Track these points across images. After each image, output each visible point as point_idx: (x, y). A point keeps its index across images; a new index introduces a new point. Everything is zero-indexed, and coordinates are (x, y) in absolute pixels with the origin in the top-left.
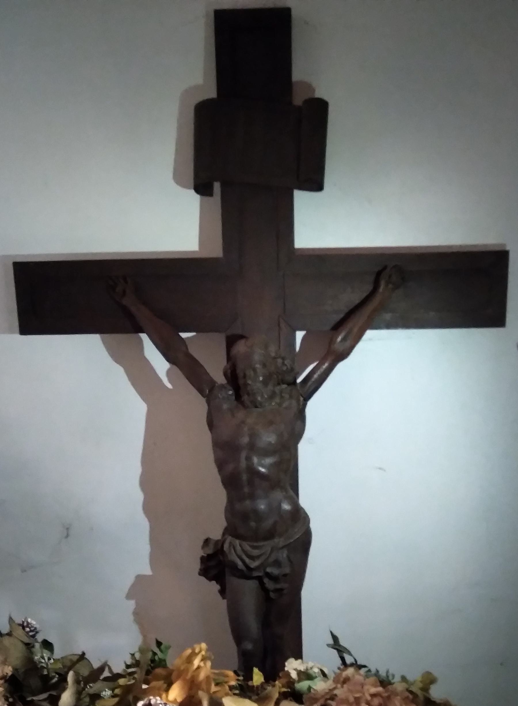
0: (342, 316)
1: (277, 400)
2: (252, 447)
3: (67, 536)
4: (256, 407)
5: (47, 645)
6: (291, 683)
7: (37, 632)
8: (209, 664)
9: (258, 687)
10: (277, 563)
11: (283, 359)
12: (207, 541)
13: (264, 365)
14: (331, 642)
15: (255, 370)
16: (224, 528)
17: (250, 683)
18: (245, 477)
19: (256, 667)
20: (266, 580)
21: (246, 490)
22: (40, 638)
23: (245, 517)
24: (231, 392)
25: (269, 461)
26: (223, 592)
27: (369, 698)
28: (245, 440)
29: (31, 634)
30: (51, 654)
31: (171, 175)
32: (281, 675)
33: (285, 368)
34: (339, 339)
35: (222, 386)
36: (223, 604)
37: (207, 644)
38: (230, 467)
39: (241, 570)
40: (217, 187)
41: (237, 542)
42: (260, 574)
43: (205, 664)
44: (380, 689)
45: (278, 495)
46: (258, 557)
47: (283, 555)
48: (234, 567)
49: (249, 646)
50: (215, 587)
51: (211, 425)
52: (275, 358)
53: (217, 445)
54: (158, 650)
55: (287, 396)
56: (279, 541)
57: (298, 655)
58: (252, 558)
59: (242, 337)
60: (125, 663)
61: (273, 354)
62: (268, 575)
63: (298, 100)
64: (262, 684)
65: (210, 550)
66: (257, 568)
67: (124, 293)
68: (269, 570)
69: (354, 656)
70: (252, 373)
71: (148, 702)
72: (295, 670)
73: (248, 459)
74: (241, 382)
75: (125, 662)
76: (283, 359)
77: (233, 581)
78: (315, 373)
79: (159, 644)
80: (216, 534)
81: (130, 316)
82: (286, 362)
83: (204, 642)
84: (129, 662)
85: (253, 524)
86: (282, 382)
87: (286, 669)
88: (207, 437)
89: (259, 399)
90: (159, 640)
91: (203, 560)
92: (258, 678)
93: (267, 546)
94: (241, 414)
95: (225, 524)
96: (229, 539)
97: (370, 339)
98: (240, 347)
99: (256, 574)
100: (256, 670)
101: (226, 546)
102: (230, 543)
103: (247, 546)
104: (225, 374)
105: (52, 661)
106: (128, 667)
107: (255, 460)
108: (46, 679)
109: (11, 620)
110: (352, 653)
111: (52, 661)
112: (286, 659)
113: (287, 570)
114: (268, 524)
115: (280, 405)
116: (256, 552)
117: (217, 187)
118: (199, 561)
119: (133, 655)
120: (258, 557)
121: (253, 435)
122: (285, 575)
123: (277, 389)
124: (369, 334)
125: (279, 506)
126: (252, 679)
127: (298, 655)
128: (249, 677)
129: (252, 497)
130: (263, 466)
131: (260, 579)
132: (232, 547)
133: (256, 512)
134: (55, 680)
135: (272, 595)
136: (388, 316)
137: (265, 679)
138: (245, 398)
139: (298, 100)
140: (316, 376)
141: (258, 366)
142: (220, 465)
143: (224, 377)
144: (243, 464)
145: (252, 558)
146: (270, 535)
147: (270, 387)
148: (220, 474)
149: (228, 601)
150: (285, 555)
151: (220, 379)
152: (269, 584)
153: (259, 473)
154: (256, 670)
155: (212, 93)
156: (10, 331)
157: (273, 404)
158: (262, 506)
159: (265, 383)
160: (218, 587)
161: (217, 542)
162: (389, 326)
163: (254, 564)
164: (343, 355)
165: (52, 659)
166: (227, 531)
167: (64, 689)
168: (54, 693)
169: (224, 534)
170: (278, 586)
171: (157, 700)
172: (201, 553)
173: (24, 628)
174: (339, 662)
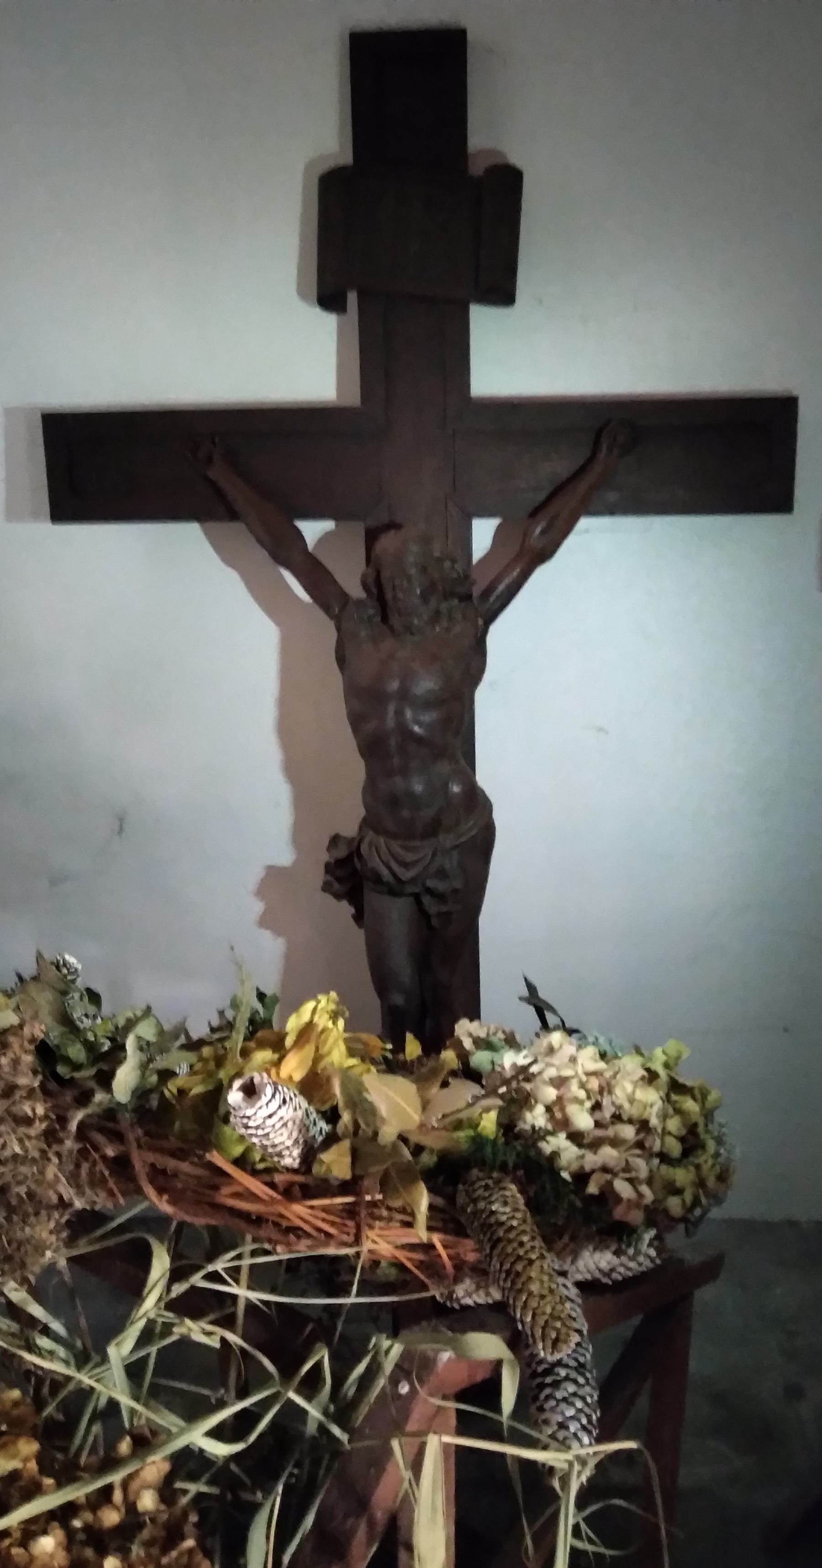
0: (542, 496)
1: (445, 623)
2: (404, 695)
3: (121, 830)
4: (412, 634)
5: (94, 997)
6: (463, 1056)
7: (78, 976)
8: (341, 1023)
9: (412, 1062)
10: (442, 874)
11: (454, 561)
12: (335, 840)
13: (423, 570)
14: (525, 992)
15: (409, 579)
16: (360, 819)
17: (401, 1057)
18: (393, 742)
19: (411, 1032)
20: (426, 900)
21: (396, 761)
22: (80, 983)
23: (394, 802)
24: (371, 612)
25: (427, 717)
26: (359, 918)
27: (584, 1078)
28: (394, 685)
29: (69, 978)
30: (97, 1010)
31: (293, 287)
32: (448, 1043)
33: (455, 576)
34: (538, 531)
35: (359, 603)
36: (358, 936)
37: (338, 995)
38: (370, 726)
39: (387, 884)
40: (352, 298)
41: (382, 840)
42: (417, 890)
43: (335, 1023)
44: (601, 1065)
45: (444, 768)
46: (414, 863)
47: (451, 863)
48: (378, 879)
49: (398, 999)
50: (346, 909)
51: (341, 660)
52: (440, 560)
53: (352, 691)
54: (261, 1005)
55: (459, 617)
56: (446, 840)
57: (474, 1014)
58: (406, 865)
59: (393, 526)
60: (209, 1023)
61: (437, 554)
62: (429, 891)
63: (477, 168)
64: (419, 1058)
65: (342, 852)
66: (413, 881)
67: (210, 460)
68: (430, 883)
69: (560, 1015)
70: (405, 584)
71: (248, 1082)
72: (470, 1035)
73: (399, 713)
74: (389, 595)
75: (258, 989)
76: (454, 561)
77: (373, 899)
78: (499, 583)
79: (261, 996)
80: (350, 829)
81: (219, 493)
82: (456, 566)
83: (333, 990)
84: (216, 1022)
85: (406, 813)
86: (447, 595)
87: (456, 1034)
88: (336, 680)
89: (416, 621)
90: (262, 989)
91: (329, 868)
92: (413, 1048)
93: (425, 850)
94: (388, 644)
95: (362, 812)
96: (370, 835)
97: (587, 531)
98: (387, 543)
99: (410, 889)
100: (409, 1037)
101: (364, 848)
102: (370, 844)
103: (396, 846)
104: (365, 585)
105: (99, 1021)
106: (213, 1030)
107: (409, 714)
108: (91, 1047)
109: (39, 957)
110: (560, 1012)
111: (99, 1021)
112: (455, 1020)
113: (458, 884)
114: (427, 814)
115: (448, 630)
116: (410, 857)
117: (352, 298)
118: (322, 869)
119: (221, 1013)
120: (414, 863)
121: (407, 678)
122: (455, 891)
123: (444, 606)
124: (584, 523)
125: (445, 786)
126: (403, 1050)
127: (474, 1014)
128: (400, 1047)
129: (405, 772)
130: (420, 724)
131: (417, 897)
132: (373, 849)
133: (410, 794)
134: (106, 1048)
135: (434, 922)
136: (612, 496)
137: (423, 1050)
138: (396, 621)
139: (477, 168)
140: (501, 587)
141: (413, 571)
142: (356, 721)
143: (361, 588)
144: (390, 721)
145: (406, 865)
146: (434, 828)
147: (433, 603)
148: (355, 737)
149: (366, 931)
150: (455, 862)
151: (356, 591)
152: (431, 906)
153: (412, 733)
154: (409, 1037)
155: (347, 158)
156: (35, 516)
157: (437, 629)
158: (418, 788)
159: (425, 597)
160: (353, 910)
161: (350, 841)
162: (612, 510)
163: (406, 875)
164: (544, 554)
165: (99, 1019)
166: (367, 823)
167: (120, 1061)
168: (105, 1067)
169: (361, 828)
170: (444, 909)
171: (262, 1078)
172: (325, 857)
173: (58, 967)
174: (538, 1024)
